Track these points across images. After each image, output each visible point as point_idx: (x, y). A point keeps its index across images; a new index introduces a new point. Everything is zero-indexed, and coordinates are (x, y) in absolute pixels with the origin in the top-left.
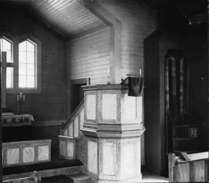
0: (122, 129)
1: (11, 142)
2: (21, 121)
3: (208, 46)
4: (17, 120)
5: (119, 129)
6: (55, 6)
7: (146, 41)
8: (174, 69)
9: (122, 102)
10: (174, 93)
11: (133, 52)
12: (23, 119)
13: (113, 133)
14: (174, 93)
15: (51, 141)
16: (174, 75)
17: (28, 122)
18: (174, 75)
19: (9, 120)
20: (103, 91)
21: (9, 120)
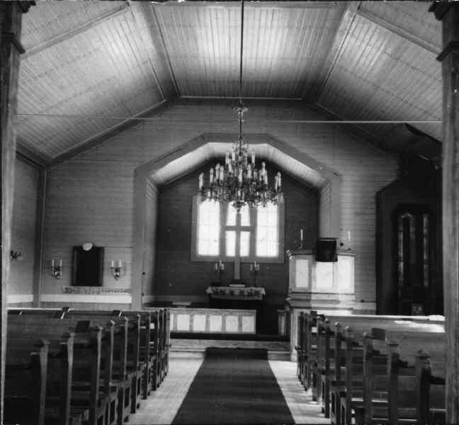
0: (312, 298)
1: (436, 314)
2: (250, 294)
3: (401, 246)
4: (246, 293)
5: (309, 298)
6: (262, 15)
7: (379, 197)
8: (412, 229)
9: (313, 269)
10: (413, 261)
11: (358, 210)
12: (253, 292)
13: (169, 324)
14: (413, 261)
15: (413, 305)
16: (412, 236)
17: (258, 296)
18: (412, 236)
19: (237, 292)
20: (297, 256)
21: (237, 292)
